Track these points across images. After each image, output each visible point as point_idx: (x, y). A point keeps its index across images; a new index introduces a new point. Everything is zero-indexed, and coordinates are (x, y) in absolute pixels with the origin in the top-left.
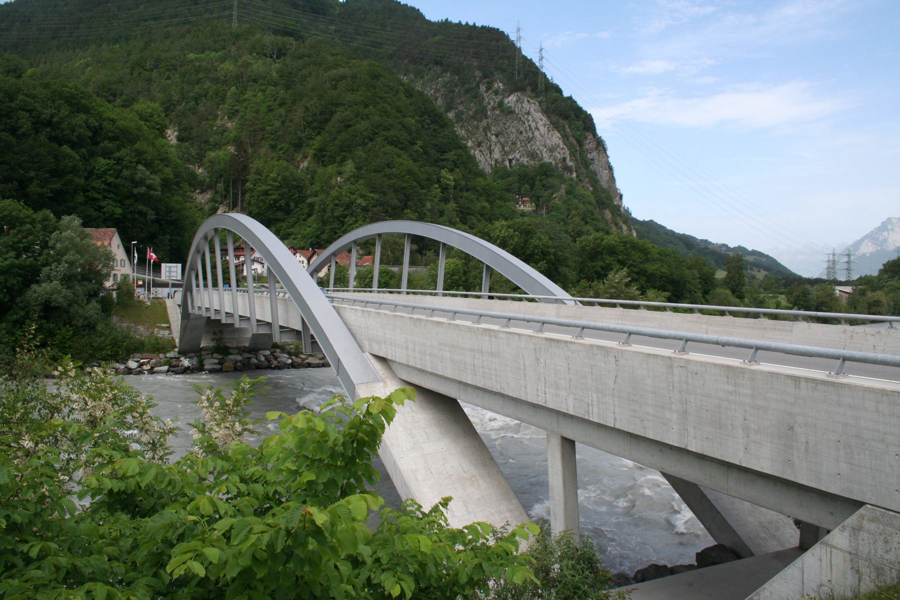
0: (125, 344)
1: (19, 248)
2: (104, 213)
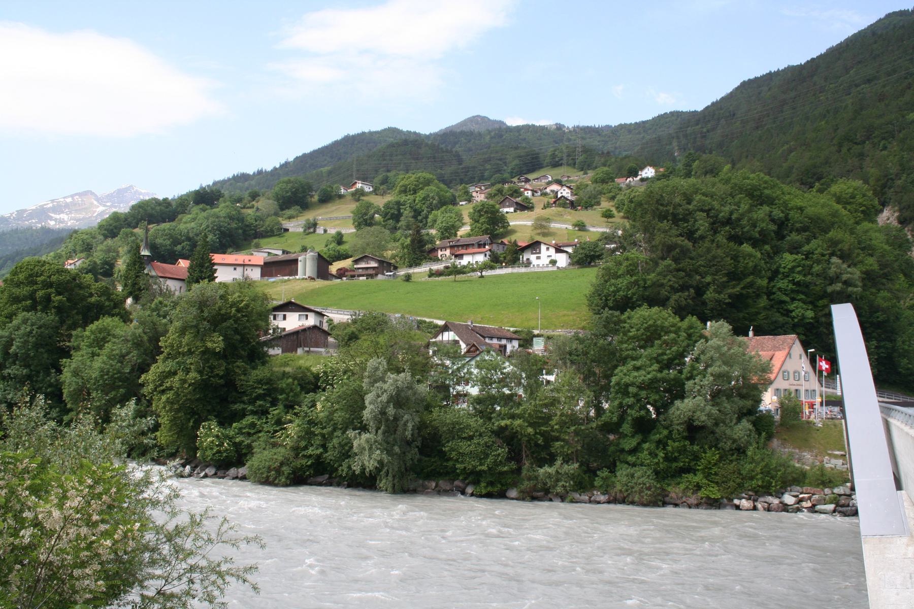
0: (779, 473)
1: (663, 360)
2: (793, 318)
